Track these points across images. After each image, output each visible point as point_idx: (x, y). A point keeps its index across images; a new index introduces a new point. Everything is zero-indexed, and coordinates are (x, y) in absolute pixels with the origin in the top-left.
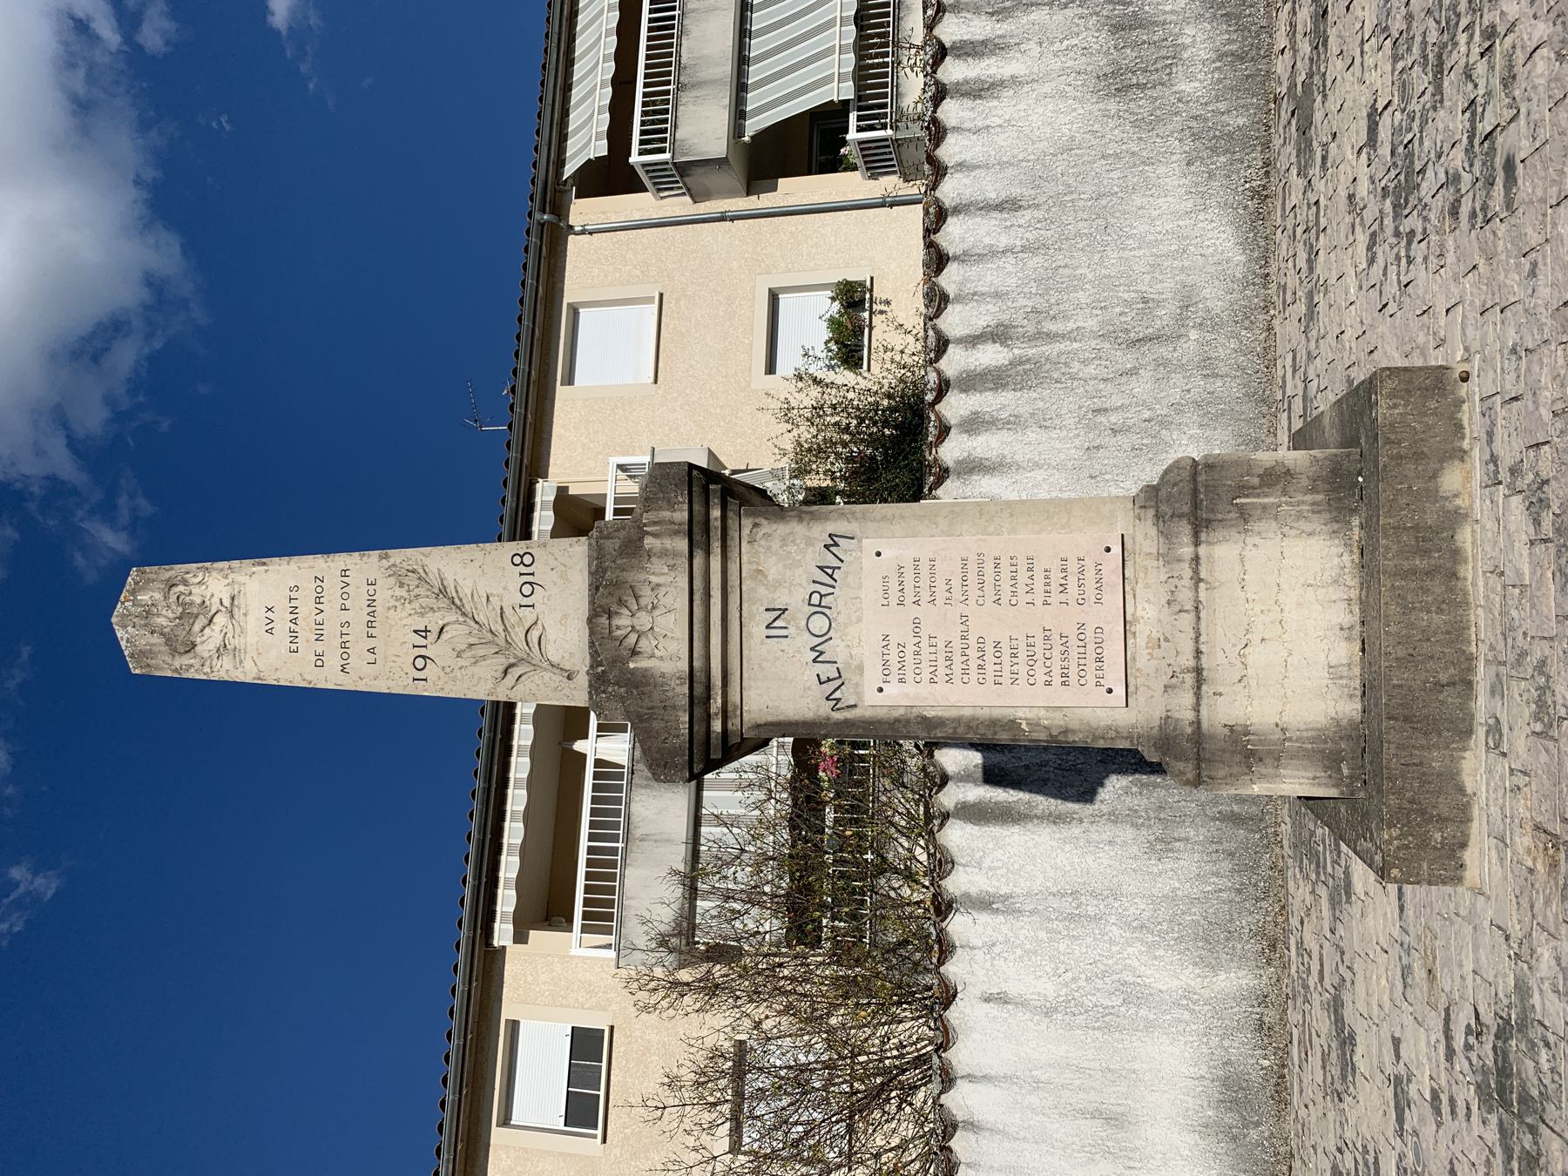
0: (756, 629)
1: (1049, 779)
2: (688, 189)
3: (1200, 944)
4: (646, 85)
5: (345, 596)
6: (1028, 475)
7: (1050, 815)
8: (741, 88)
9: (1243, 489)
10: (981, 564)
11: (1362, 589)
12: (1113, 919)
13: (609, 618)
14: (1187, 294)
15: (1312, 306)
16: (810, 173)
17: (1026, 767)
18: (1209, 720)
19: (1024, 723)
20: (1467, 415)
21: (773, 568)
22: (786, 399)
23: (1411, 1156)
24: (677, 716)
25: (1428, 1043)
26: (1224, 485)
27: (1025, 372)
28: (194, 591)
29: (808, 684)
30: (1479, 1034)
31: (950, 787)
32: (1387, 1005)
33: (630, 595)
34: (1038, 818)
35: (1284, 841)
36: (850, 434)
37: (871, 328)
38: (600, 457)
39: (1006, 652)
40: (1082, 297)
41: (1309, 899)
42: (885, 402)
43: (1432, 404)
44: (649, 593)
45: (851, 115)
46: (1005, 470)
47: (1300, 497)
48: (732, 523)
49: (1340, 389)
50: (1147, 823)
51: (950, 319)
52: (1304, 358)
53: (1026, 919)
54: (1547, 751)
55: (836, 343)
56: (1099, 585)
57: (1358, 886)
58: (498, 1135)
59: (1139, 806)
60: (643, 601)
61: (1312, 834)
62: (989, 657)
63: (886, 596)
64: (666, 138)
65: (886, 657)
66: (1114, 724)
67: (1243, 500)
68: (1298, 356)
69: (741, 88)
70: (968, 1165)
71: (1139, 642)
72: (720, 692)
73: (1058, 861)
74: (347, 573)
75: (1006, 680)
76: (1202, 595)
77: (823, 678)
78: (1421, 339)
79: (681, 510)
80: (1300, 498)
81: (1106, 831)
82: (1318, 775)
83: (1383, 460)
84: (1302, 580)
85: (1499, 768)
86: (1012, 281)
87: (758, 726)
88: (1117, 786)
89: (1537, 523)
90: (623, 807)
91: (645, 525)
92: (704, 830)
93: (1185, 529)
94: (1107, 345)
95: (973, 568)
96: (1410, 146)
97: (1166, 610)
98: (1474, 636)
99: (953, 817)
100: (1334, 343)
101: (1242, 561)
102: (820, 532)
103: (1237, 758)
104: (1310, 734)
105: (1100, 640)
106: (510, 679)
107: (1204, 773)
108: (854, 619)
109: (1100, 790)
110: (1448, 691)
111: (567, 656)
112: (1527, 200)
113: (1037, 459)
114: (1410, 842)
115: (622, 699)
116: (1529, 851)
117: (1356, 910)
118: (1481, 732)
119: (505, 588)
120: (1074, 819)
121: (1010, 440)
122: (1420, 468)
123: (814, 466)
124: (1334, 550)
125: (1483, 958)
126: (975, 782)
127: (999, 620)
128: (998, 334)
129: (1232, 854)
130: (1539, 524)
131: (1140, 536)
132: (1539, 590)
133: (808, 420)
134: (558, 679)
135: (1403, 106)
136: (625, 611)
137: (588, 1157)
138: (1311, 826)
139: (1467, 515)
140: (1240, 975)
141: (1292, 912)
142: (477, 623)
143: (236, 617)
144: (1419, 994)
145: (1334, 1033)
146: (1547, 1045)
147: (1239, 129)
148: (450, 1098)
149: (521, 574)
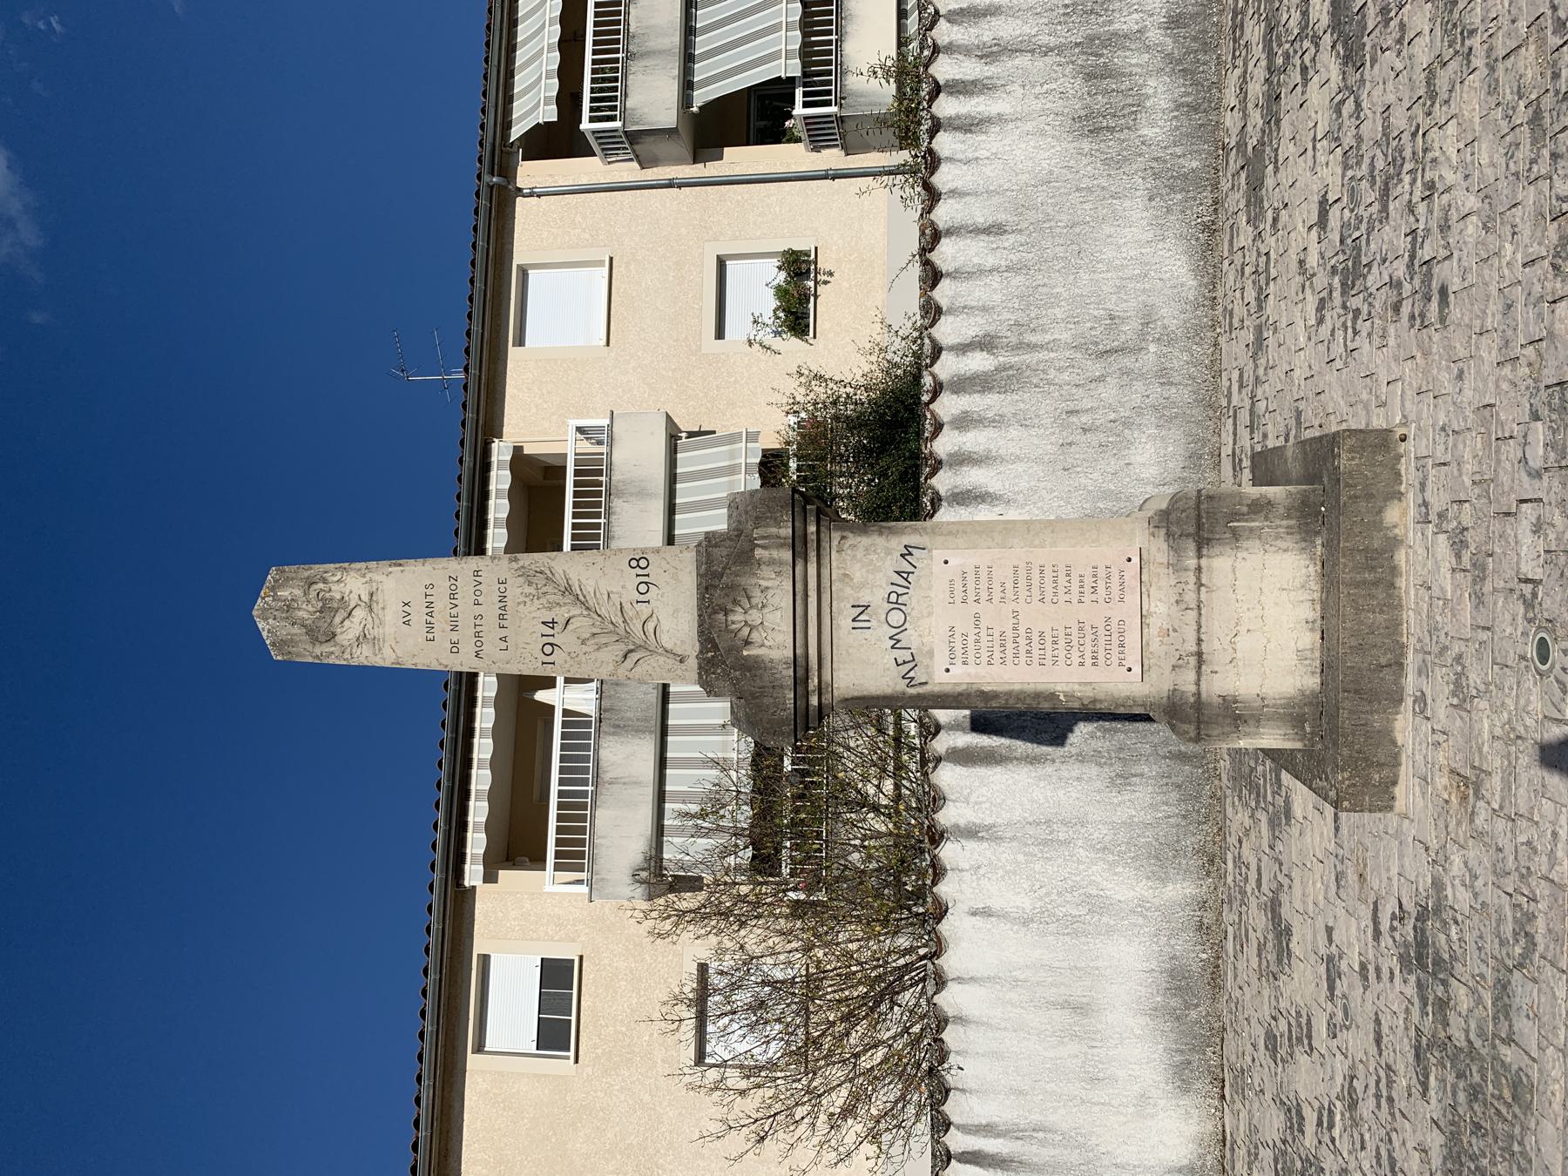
0: (844, 622)
1: (1026, 727)
2: (637, 156)
3: (1152, 861)
4: (595, 52)
5: (477, 593)
7: (1027, 757)
8: (688, 58)
9: (1236, 516)
10: (1029, 570)
12: (1080, 843)
13: (726, 615)
14: (1146, 313)
15: (1260, 342)
16: (748, 144)
19: (1062, 695)
21: (858, 573)
23: (1340, 1014)
25: (1358, 928)
27: (1008, 377)
28: (333, 588)
30: (1402, 919)
31: (942, 735)
32: (1322, 902)
34: (1017, 759)
37: (816, 297)
38: (555, 417)
39: (1049, 639)
40: (1059, 313)
41: (1247, 822)
44: (759, 594)
45: (797, 91)
47: (1278, 522)
50: (1109, 762)
51: (943, 329)
52: (1251, 379)
53: (1006, 844)
54: (1461, 718)
55: (784, 310)
57: (1298, 811)
58: (473, 1061)
60: (754, 601)
61: (1252, 770)
62: (1035, 645)
64: (616, 106)
67: (1235, 524)
69: (688, 58)
70: (957, 1053)
73: (1034, 795)
74: (480, 573)
75: (1048, 662)
76: (1203, 596)
77: (900, 661)
78: (1365, 396)
79: (787, 527)
81: (1075, 769)
83: (1343, 499)
84: (1278, 585)
85: (1423, 728)
86: (998, 297)
89: (1458, 556)
90: (592, 753)
93: (1191, 546)
94: (1079, 355)
95: (1022, 574)
96: (1358, 241)
97: (1175, 608)
98: (1405, 631)
101: (1234, 571)
102: (897, 543)
103: (1228, 721)
104: (1283, 701)
109: (1070, 735)
110: (1386, 671)
111: (679, 643)
112: (1456, 322)
116: (1446, 788)
117: (1295, 831)
118: (1410, 701)
126: (963, 730)
127: (1043, 614)
128: (985, 344)
129: (1179, 786)
130: (1460, 557)
131: (1153, 550)
132: (1459, 604)
134: (671, 662)
135: (1352, 206)
137: (561, 1077)
139: (1402, 541)
140: (1184, 885)
141: (1230, 833)
142: (599, 616)
143: (375, 610)
144: (1351, 894)
145: (1271, 927)
146: (1456, 922)
147: (1193, 171)
148: (429, 1028)
149: (637, 575)
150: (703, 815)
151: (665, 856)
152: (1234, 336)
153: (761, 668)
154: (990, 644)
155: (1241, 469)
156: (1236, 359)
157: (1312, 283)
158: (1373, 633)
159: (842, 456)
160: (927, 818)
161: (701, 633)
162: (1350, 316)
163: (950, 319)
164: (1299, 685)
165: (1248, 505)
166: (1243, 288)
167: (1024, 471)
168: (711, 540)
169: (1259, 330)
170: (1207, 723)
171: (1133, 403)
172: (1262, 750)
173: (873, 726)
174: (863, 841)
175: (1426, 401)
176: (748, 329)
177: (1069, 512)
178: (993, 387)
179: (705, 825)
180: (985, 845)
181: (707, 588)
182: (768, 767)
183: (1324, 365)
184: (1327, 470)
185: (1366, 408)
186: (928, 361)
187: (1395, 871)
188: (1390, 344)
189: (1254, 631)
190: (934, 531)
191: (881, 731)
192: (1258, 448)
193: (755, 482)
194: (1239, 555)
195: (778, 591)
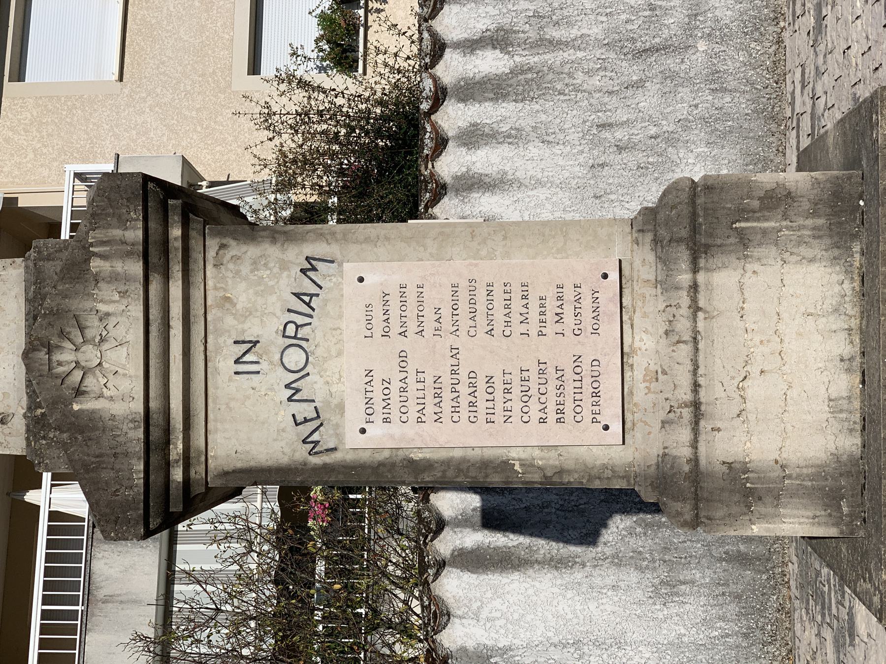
0: (224, 364)
1: (550, 521)
6: (530, 193)
7: (551, 559)
9: (743, 213)
10: (472, 291)
11: (862, 318)
13: (49, 353)
15: (820, 19)
17: (527, 509)
18: (707, 457)
19: (517, 463)
21: (242, 295)
22: (266, 103)
24: (130, 464)
26: (724, 208)
29: (282, 425)
31: (447, 534)
33: (73, 326)
34: (539, 563)
35: (791, 582)
36: (340, 144)
37: (367, 28)
38: (55, 164)
39: (499, 387)
41: (815, 641)
42: (378, 111)
44: (96, 323)
46: (507, 187)
47: (801, 221)
48: (195, 243)
49: (846, 106)
50: (651, 565)
51: (446, 21)
52: (812, 73)
55: (328, 42)
56: (596, 314)
60: (89, 333)
61: (818, 573)
62: (481, 394)
63: (369, 326)
65: (369, 395)
66: (611, 462)
67: (743, 225)
68: (807, 71)
71: (637, 376)
72: (181, 436)
75: (499, 418)
76: (701, 325)
77: (300, 419)
79: (135, 228)
80: (801, 222)
81: (609, 576)
82: (818, 513)
84: (803, 309)
87: (226, 474)
88: (621, 527)
90: (83, 565)
91: (91, 245)
92: (177, 588)
93: (683, 255)
94: (612, 55)
95: (463, 296)
97: (664, 341)
99: (450, 565)
100: (840, 58)
101: (741, 289)
102: (296, 254)
104: (810, 470)
105: (597, 374)
107: (702, 514)
108: (334, 353)
113: (539, 176)
115: (64, 446)
117: (859, 653)
120: (576, 563)
123: (299, 179)
124: (835, 278)
126: (473, 527)
129: (738, 597)
131: (637, 263)
133: (291, 128)
136: (68, 345)
138: (817, 566)
141: (799, 656)
152: (797, 27)
153: (98, 429)
154: (420, 394)
164: (832, 447)
165: (759, 199)
167: (547, 199)
170: (708, 500)
178: (508, 94)
189: (771, 371)
195: (124, 319)
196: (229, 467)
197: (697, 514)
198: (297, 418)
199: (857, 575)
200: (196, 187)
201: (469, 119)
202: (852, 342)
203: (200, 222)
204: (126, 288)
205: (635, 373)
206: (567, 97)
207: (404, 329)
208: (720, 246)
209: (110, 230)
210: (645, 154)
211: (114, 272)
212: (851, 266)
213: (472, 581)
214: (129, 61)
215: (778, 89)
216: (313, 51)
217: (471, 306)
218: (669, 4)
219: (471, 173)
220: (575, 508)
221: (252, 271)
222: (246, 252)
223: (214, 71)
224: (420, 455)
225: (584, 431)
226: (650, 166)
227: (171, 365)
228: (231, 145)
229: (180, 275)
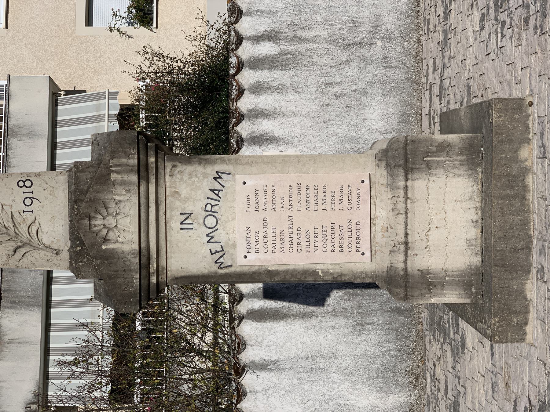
0: (175, 224)
1: (300, 294)
3: (380, 380)
6: (289, 119)
7: (300, 314)
9: (428, 153)
10: (299, 189)
11: (482, 202)
12: (334, 370)
13: (90, 220)
14: (375, 20)
15: (446, 40)
18: (411, 267)
19: (320, 272)
20: (531, 122)
21: (184, 190)
27: (287, 59)
29: (205, 255)
31: (244, 302)
32: (484, 402)
33: (102, 207)
39: (312, 235)
41: (439, 352)
43: (517, 117)
44: (114, 205)
46: (276, 116)
47: (455, 158)
48: (161, 165)
50: (352, 315)
51: (243, 25)
52: (441, 64)
53: (286, 373)
55: (135, 8)
56: (358, 200)
57: (469, 345)
59: (348, 306)
60: (110, 210)
61: (442, 318)
62: (303, 238)
63: (249, 206)
65: (248, 239)
66: (365, 270)
67: (428, 159)
71: (378, 229)
72: (155, 261)
75: (312, 250)
76: (409, 206)
77: (213, 251)
78: (508, 77)
79: (133, 158)
80: (455, 158)
81: (330, 321)
83: (495, 143)
84: (455, 198)
85: (543, 288)
88: (337, 296)
91: (111, 166)
94: (333, 47)
97: (391, 213)
98: (532, 227)
99: (246, 318)
100: (460, 64)
101: (428, 189)
102: (211, 170)
103: (424, 286)
105: (359, 228)
106: (18, 256)
107: (408, 294)
109: (328, 299)
111: (55, 241)
113: (294, 110)
114: (503, 324)
117: (467, 356)
118: (534, 271)
119: (13, 201)
120: (313, 315)
121: (279, 99)
122: (510, 147)
124: (470, 184)
125: (533, 375)
126: (258, 298)
129: (396, 330)
131: (378, 175)
136: (100, 216)
144: (501, 395)
149: (24, 192)
150: (76, 363)
151: (50, 393)
152: (430, 37)
154: (274, 239)
155: (434, 124)
156: (431, 52)
157: (477, 3)
158: (513, 228)
159: (175, 110)
160: (234, 358)
161: (71, 233)
162: (500, 25)
163: (248, 18)
166: (436, 5)
168: (78, 167)
169: (445, 33)
171: (367, 79)
172: (446, 304)
173: (198, 296)
174: (190, 376)
175: (544, 80)
176: (110, 20)
177: (327, 150)
178: (277, 66)
179: (78, 370)
180: (272, 374)
181: (76, 202)
182: (124, 327)
183: (484, 56)
184: (485, 124)
185: (509, 84)
186: (234, 46)
187: (526, 380)
188: (523, 44)
190: (236, 162)
191: (203, 300)
192: (444, 110)
193: (116, 126)
194: (431, 178)
195: (128, 203)
196: (179, 275)
197: (406, 294)
198: (212, 251)
199: (477, 320)
200: (57, 95)
201: (256, 79)
202: (477, 214)
203: (162, 154)
204: (129, 188)
205: (377, 228)
206: (309, 68)
207: (266, 207)
208: (418, 169)
209: (120, 159)
210: (350, 100)
211: (123, 180)
212: (477, 178)
213: (258, 326)
214: (11, 16)
215: (418, 67)
216: (125, 13)
217: (299, 196)
218: (362, 20)
219: (257, 108)
220: (313, 287)
221: (189, 178)
222: (186, 169)
223: (64, 23)
224: (273, 268)
225: (353, 256)
226: (352, 106)
227: (150, 225)
228: (76, 69)
229: (154, 181)
